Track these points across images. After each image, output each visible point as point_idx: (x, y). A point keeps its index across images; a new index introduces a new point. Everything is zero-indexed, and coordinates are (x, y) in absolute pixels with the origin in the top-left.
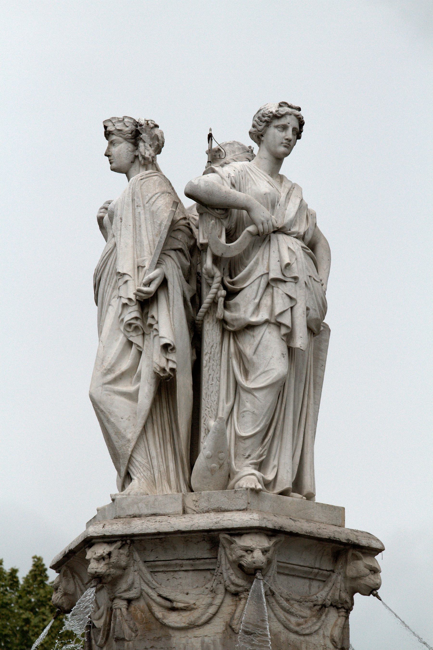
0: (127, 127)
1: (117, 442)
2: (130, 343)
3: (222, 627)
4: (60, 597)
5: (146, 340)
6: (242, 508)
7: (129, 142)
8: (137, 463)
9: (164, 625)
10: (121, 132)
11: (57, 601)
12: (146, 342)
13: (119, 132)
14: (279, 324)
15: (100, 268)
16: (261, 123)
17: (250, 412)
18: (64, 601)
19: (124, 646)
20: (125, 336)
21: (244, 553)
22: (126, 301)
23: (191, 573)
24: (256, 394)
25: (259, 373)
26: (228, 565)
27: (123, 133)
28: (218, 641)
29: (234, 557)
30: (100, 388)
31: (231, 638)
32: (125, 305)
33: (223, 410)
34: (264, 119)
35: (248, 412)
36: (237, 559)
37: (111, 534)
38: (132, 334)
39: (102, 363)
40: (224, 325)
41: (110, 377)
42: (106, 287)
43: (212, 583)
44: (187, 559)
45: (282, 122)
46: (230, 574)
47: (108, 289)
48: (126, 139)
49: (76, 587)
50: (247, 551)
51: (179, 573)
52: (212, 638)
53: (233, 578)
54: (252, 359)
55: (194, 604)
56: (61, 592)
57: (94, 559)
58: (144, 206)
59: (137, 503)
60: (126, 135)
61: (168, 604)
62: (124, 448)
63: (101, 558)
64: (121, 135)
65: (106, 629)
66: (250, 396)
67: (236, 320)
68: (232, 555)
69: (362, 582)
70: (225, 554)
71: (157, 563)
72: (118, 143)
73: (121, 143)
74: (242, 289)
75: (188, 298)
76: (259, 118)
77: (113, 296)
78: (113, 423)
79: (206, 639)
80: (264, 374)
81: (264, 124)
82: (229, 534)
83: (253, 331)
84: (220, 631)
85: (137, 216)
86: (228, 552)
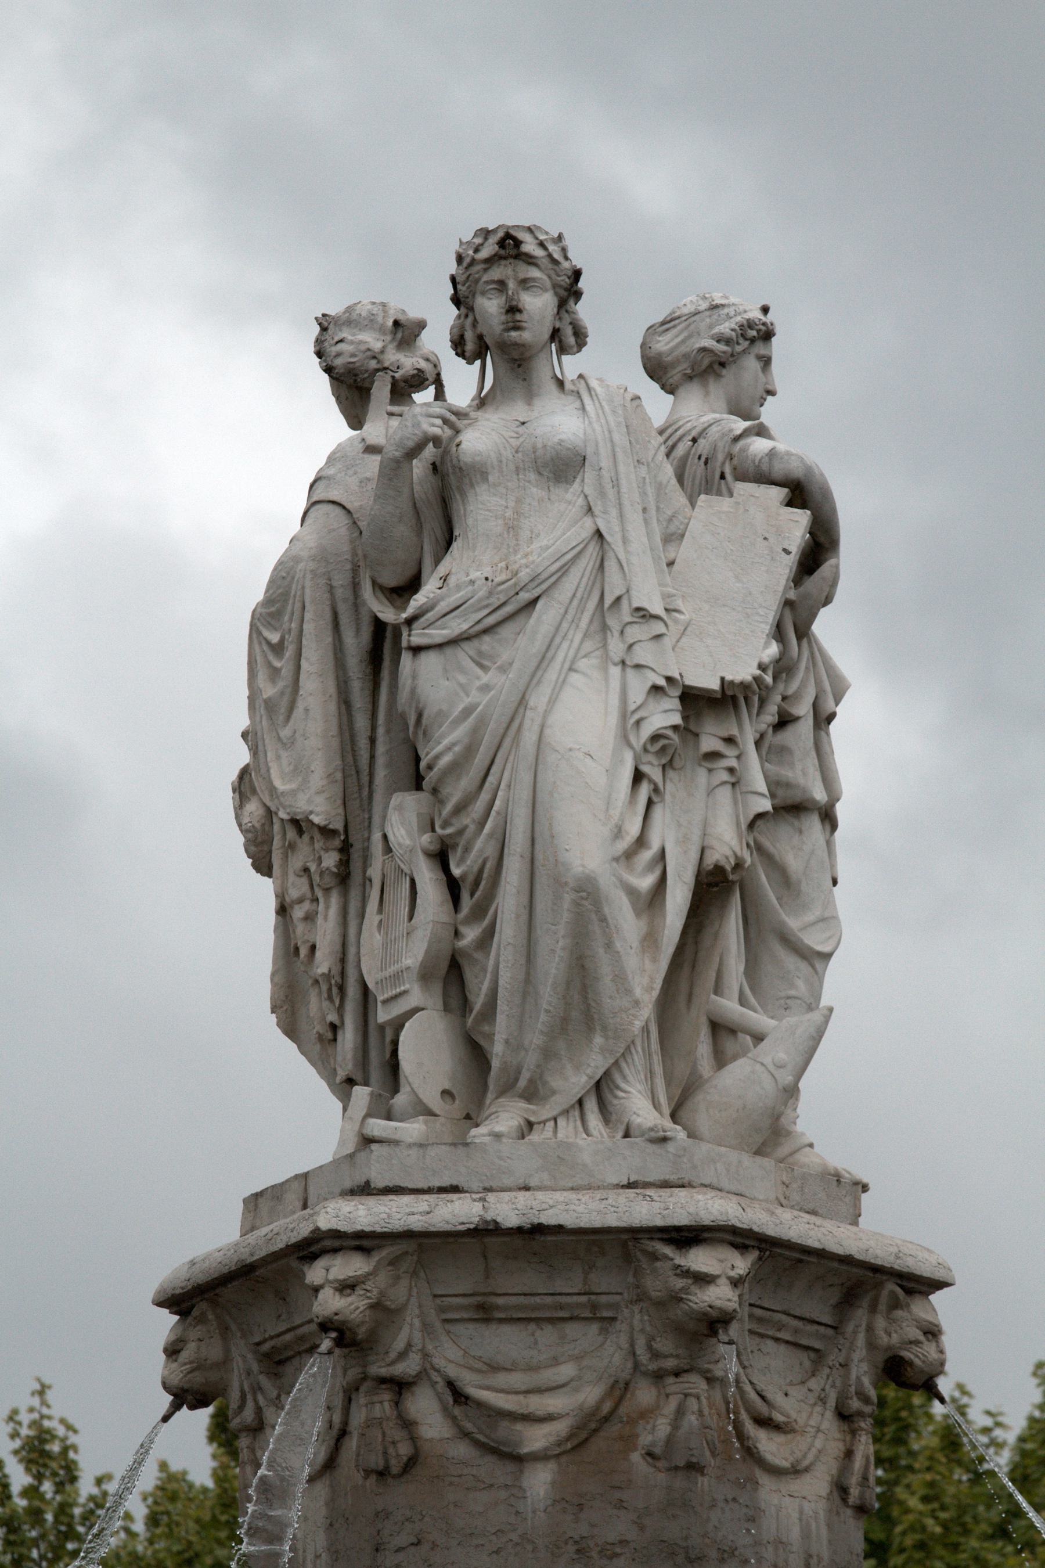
1: (611, 997)
2: (638, 777)
4: (362, 1308)
5: (671, 780)
9: (751, 1453)
10: (556, 267)
11: (353, 1316)
12: (669, 786)
13: (550, 266)
16: (741, 341)
17: (805, 1002)
18: (367, 1319)
19: (697, 1483)
20: (637, 759)
21: (922, 1338)
22: (662, 682)
23: (783, 1348)
27: (558, 270)
28: (821, 1513)
29: (895, 1339)
30: (607, 865)
32: (656, 689)
35: (799, 1002)
36: (898, 1345)
37: (760, 1231)
44: (795, 1317)
47: (571, 632)
49: (410, 1295)
56: (369, 1298)
57: (729, 1278)
60: (562, 278)
62: (624, 1016)
64: (552, 273)
65: (593, 1426)
66: (803, 966)
70: (870, 1329)
72: (541, 289)
75: (805, 727)
77: (582, 653)
78: (618, 952)
80: (821, 924)
81: (747, 343)
82: (901, 1287)
83: (798, 817)
86: (880, 1323)
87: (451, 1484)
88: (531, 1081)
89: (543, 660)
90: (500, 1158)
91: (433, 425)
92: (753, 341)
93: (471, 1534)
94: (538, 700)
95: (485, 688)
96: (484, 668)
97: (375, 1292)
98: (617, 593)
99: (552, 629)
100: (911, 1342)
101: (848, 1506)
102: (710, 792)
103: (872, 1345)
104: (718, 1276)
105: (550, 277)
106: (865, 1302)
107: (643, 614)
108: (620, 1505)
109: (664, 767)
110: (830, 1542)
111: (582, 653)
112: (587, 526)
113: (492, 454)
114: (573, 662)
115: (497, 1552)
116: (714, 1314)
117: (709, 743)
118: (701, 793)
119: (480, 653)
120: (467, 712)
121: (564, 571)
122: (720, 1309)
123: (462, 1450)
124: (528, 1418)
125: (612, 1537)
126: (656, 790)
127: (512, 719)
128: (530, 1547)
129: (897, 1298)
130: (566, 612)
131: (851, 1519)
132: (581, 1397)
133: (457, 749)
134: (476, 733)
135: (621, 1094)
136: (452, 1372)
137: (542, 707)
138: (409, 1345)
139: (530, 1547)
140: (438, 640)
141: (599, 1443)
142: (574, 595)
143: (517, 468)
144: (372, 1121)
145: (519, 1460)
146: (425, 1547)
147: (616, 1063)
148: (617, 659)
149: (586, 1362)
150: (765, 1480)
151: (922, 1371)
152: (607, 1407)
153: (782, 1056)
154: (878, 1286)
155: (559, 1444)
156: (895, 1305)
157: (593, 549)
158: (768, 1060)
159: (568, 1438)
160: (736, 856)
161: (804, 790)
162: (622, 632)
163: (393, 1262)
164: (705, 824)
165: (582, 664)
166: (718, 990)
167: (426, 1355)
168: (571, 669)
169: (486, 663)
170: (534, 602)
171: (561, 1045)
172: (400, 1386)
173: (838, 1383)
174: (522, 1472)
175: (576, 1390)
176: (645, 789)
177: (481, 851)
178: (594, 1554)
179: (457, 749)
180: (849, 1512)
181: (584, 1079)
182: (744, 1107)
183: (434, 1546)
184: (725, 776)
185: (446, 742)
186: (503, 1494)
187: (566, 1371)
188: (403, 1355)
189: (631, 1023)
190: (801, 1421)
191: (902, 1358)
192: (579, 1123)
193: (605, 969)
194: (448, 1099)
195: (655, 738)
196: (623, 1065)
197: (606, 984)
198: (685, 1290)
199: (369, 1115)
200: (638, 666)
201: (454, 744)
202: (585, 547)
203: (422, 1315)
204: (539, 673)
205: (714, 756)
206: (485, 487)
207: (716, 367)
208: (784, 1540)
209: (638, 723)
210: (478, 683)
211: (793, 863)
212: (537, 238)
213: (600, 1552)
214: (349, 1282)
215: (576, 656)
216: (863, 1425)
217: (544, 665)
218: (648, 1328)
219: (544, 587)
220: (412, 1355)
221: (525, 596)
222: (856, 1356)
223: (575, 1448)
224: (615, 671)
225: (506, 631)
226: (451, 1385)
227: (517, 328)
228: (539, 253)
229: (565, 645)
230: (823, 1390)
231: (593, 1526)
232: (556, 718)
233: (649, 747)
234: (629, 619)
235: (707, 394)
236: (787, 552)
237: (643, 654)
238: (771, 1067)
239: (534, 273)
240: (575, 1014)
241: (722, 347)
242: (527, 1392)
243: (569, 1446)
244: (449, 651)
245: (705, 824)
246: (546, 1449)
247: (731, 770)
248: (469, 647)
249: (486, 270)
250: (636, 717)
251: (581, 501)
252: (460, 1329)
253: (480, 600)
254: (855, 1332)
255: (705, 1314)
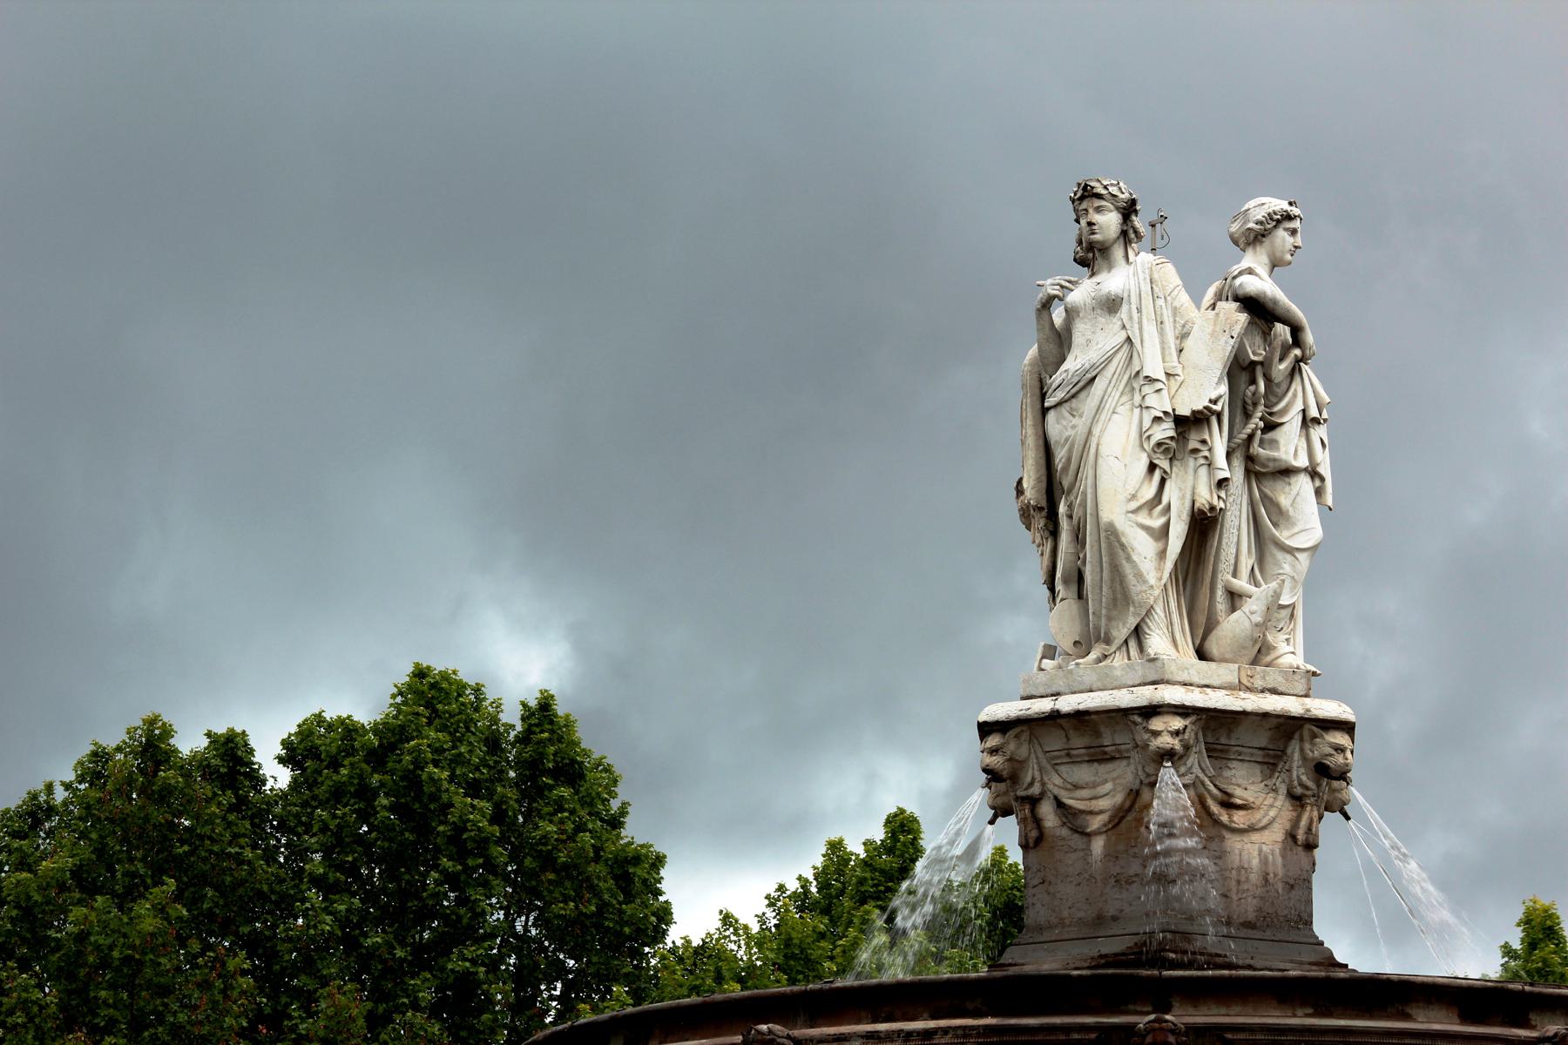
0: (1123, 193)
2: (1152, 467)
3: (1281, 835)
6: (1300, 694)
7: (1119, 212)
8: (1155, 616)
12: (1174, 469)
14: (1313, 473)
15: (1098, 364)
16: (1270, 221)
20: (1149, 456)
21: (1334, 752)
22: (1161, 415)
23: (1246, 764)
24: (1297, 555)
25: (1296, 530)
26: (1300, 762)
28: (1278, 851)
31: (1291, 850)
32: (1157, 419)
33: (1246, 567)
34: (1276, 217)
38: (1158, 455)
39: (1124, 486)
40: (1250, 463)
41: (1134, 505)
42: (1110, 389)
43: (1274, 780)
45: (1292, 225)
46: (1300, 773)
48: (1117, 208)
49: (1030, 753)
50: (1336, 750)
51: (1233, 762)
52: (1270, 847)
53: (1304, 778)
54: (1288, 511)
55: (1253, 802)
58: (1165, 298)
59: (1187, 669)
61: (1225, 798)
63: (1177, 733)
65: (1121, 814)
66: (1289, 557)
67: (1275, 460)
68: (1313, 752)
69: (1340, 796)
70: (1302, 750)
71: (1215, 746)
73: (1112, 211)
74: (1282, 424)
76: (1269, 214)
77: (1121, 402)
79: (1265, 848)
81: (1274, 223)
83: (1288, 477)
84: (1280, 840)
85: (1158, 310)
86: (1307, 746)
87: (1058, 850)
88: (1106, 633)
89: (1099, 409)
90: (1079, 676)
91: (1054, 289)
92: (1278, 221)
93: (1067, 876)
94: (1096, 431)
95: (1074, 427)
96: (1073, 416)
97: (1008, 752)
98: (1137, 369)
99: (1102, 393)
100: (1327, 755)
101: (1299, 846)
102: (1195, 471)
103: (1304, 758)
104: (1162, 731)
105: (1112, 204)
106: (1297, 736)
107: (1150, 380)
108: (1135, 856)
109: (1171, 459)
110: (1284, 865)
111: (1121, 402)
112: (1123, 335)
113: (1082, 302)
114: (1115, 408)
115: (1079, 884)
116: (1162, 751)
117: (1193, 444)
118: (1191, 471)
119: (1071, 408)
120: (1067, 440)
121: (1109, 360)
122: (1163, 748)
123: (1065, 832)
124: (1091, 813)
125: (1132, 872)
126: (1165, 472)
127: (1085, 446)
128: (1094, 881)
129: (1313, 732)
130: (1110, 382)
131: (1302, 853)
132: (1115, 799)
133: (1063, 460)
134: (1070, 451)
135: (1147, 636)
136: (1056, 791)
137: (1097, 434)
138: (1033, 779)
139: (1094, 881)
140: (1053, 404)
141: (1123, 825)
142: (1115, 373)
143: (1093, 308)
144: (1045, 661)
145: (1089, 835)
146: (1046, 884)
147: (1143, 620)
148: (1137, 404)
149: (1118, 781)
150: (1227, 835)
151: (1336, 771)
152: (1128, 804)
153: (1254, 608)
154: (1301, 727)
155: (1105, 825)
156: (1314, 736)
157: (1126, 348)
158: (1247, 611)
159: (1110, 822)
160: (1209, 502)
161: (1286, 461)
162: (1140, 390)
163: (1016, 736)
164: (1194, 488)
165: (1119, 409)
166: (1235, 575)
167: (1043, 784)
168: (1114, 412)
169: (1074, 413)
170: (1094, 378)
171: (1115, 613)
172: (1034, 802)
173: (1287, 780)
174: (1090, 841)
175: (1114, 796)
176: (1157, 475)
177: (1077, 513)
178: (1123, 883)
179: (1063, 460)
180: (1300, 849)
181: (1126, 630)
182: (1234, 637)
183: (1050, 883)
184: (1202, 461)
185: (1059, 457)
186: (1082, 854)
187: (1109, 786)
188: (1031, 784)
189: (1148, 598)
190: (1258, 803)
191: (1324, 764)
192: (1125, 654)
193: (1127, 569)
194: (1078, 645)
195: (1159, 444)
196: (1148, 620)
197: (1131, 579)
198: (1148, 740)
199: (1043, 657)
200: (1147, 407)
201: (1062, 458)
202: (1122, 346)
203: (1039, 763)
204: (1097, 416)
205: (1195, 451)
206: (1078, 319)
207: (1260, 237)
208: (1246, 866)
209: (1149, 437)
210: (1071, 424)
211: (1284, 501)
212: (1102, 184)
213: (1126, 882)
214: (993, 748)
215: (1117, 404)
216: (1308, 801)
217: (1099, 411)
218: (1142, 761)
219: (1098, 370)
220: (1036, 784)
221: (1089, 376)
222: (1295, 765)
223: (1113, 827)
224: (1137, 411)
225: (1082, 395)
226: (1056, 798)
227: (1094, 234)
228: (1103, 192)
229: (1110, 400)
230: (1275, 784)
231: (1122, 867)
232: (1103, 441)
233: (1156, 450)
234: (1142, 383)
235: (1255, 252)
236: (1232, 337)
237: (1149, 402)
238: (1248, 613)
239: (1103, 203)
240: (1119, 596)
241: (1258, 227)
242: (1091, 799)
243: (1110, 826)
244: (1059, 408)
245: (1194, 488)
246: (1099, 828)
247: (1206, 458)
248: (1066, 406)
249: (1080, 204)
250: (1147, 435)
251: (1120, 323)
252: (1062, 769)
253: (1068, 381)
254: (1293, 752)
255: (1158, 752)
